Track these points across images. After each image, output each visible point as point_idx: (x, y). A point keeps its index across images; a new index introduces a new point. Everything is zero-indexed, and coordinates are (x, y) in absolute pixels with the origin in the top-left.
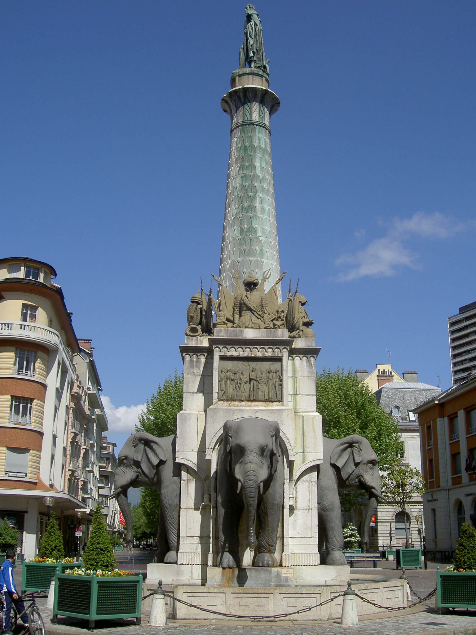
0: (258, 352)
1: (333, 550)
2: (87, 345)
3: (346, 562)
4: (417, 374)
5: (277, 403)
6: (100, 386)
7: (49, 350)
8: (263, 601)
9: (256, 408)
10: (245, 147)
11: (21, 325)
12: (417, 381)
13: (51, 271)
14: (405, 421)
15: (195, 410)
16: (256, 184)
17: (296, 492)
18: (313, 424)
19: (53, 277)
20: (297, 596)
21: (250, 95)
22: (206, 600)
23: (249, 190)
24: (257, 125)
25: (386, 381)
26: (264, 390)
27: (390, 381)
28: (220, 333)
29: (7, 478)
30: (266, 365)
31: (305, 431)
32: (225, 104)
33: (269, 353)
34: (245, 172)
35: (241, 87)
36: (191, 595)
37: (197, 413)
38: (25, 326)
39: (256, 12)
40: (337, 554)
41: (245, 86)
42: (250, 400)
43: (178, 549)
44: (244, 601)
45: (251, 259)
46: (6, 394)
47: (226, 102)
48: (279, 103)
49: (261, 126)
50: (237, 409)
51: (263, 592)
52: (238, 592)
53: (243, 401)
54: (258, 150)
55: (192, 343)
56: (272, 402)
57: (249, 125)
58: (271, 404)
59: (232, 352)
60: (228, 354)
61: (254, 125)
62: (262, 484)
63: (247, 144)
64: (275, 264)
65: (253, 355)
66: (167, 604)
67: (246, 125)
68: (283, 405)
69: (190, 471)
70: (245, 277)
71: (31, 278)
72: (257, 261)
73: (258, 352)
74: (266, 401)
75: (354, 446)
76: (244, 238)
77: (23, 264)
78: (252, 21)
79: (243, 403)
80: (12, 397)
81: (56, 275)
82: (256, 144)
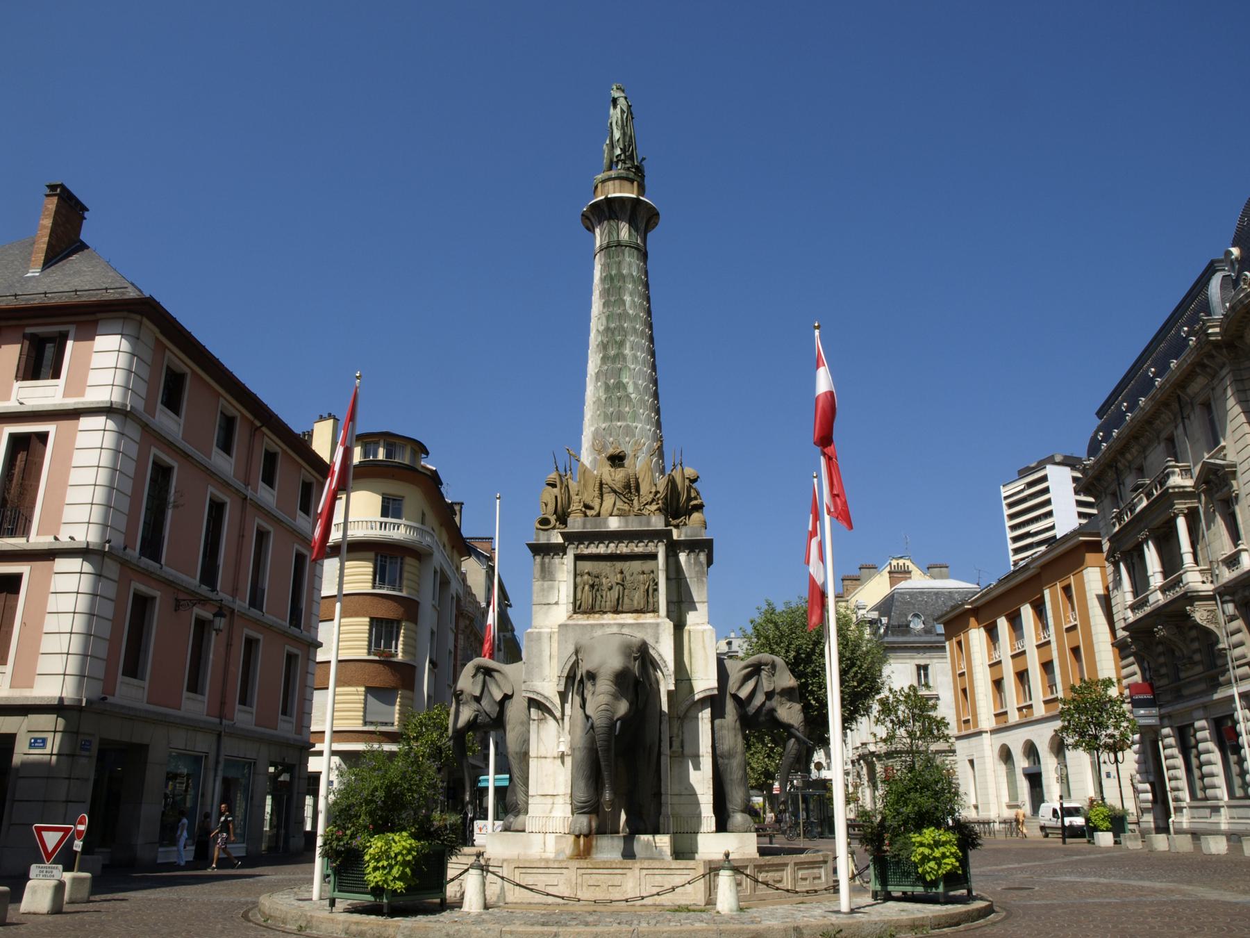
0: (624, 548)
1: (733, 812)
2: (486, 545)
3: (753, 829)
4: (947, 567)
5: (651, 615)
6: (508, 601)
7: (420, 555)
8: (617, 880)
9: (622, 622)
10: (611, 275)
11: (381, 523)
12: (947, 577)
13: (420, 449)
14: (297, 630)
15: (547, 627)
16: (625, 325)
17: (683, 733)
18: (703, 641)
19: (423, 456)
20: (664, 872)
21: (616, 206)
22: (543, 877)
23: (616, 333)
24: (626, 246)
25: (901, 580)
26: (586, 596)
27: (906, 579)
28: (576, 524)
29: (366, 728)
30: (636, 565)
31: (692, 651)
32: (587, 220)
33: (640, 548)
34: (611, 309)
35: (603, 197)
36: (524, 871)
37: (549, 630)
38: (386, 524)
39: (623, 95)
40: (738, 818)
41: (609, 196)
42: (616, 612)
43: (526, 812)
44: (593, 880)
45: (619, 424)
46: (364, 616)
47: (587, 218)
48: (657, 214)
49: (632, 247)
50: (597, 625)
51: (618, 866)
52: (585, 866)
53: (605, 613)
54: (628, 280)
55: (543, 539)
56: (644, 613)
57: (616, 246)
58: (643, 615)
59: (593, 550)
60: (586, 552)
61: (622, 246)
62: (618, 724)
63: (613, 272)
64: (653, 429)
65: (618, 552)
66: (876, 924)
67: (612, 247)
68: (658, 616)
69: (541, 707)
70: (611, 451)
71: (371, 458)
72: (628, 426)
73: (624, 548)
74: (636, 611)
75: (763, 669)
76: (611, 397)
77: (382, 443)
78: (619, 106)
79: (605, 616)
80: (372, 619)
81: (427, 453)
82: (624, 272)
